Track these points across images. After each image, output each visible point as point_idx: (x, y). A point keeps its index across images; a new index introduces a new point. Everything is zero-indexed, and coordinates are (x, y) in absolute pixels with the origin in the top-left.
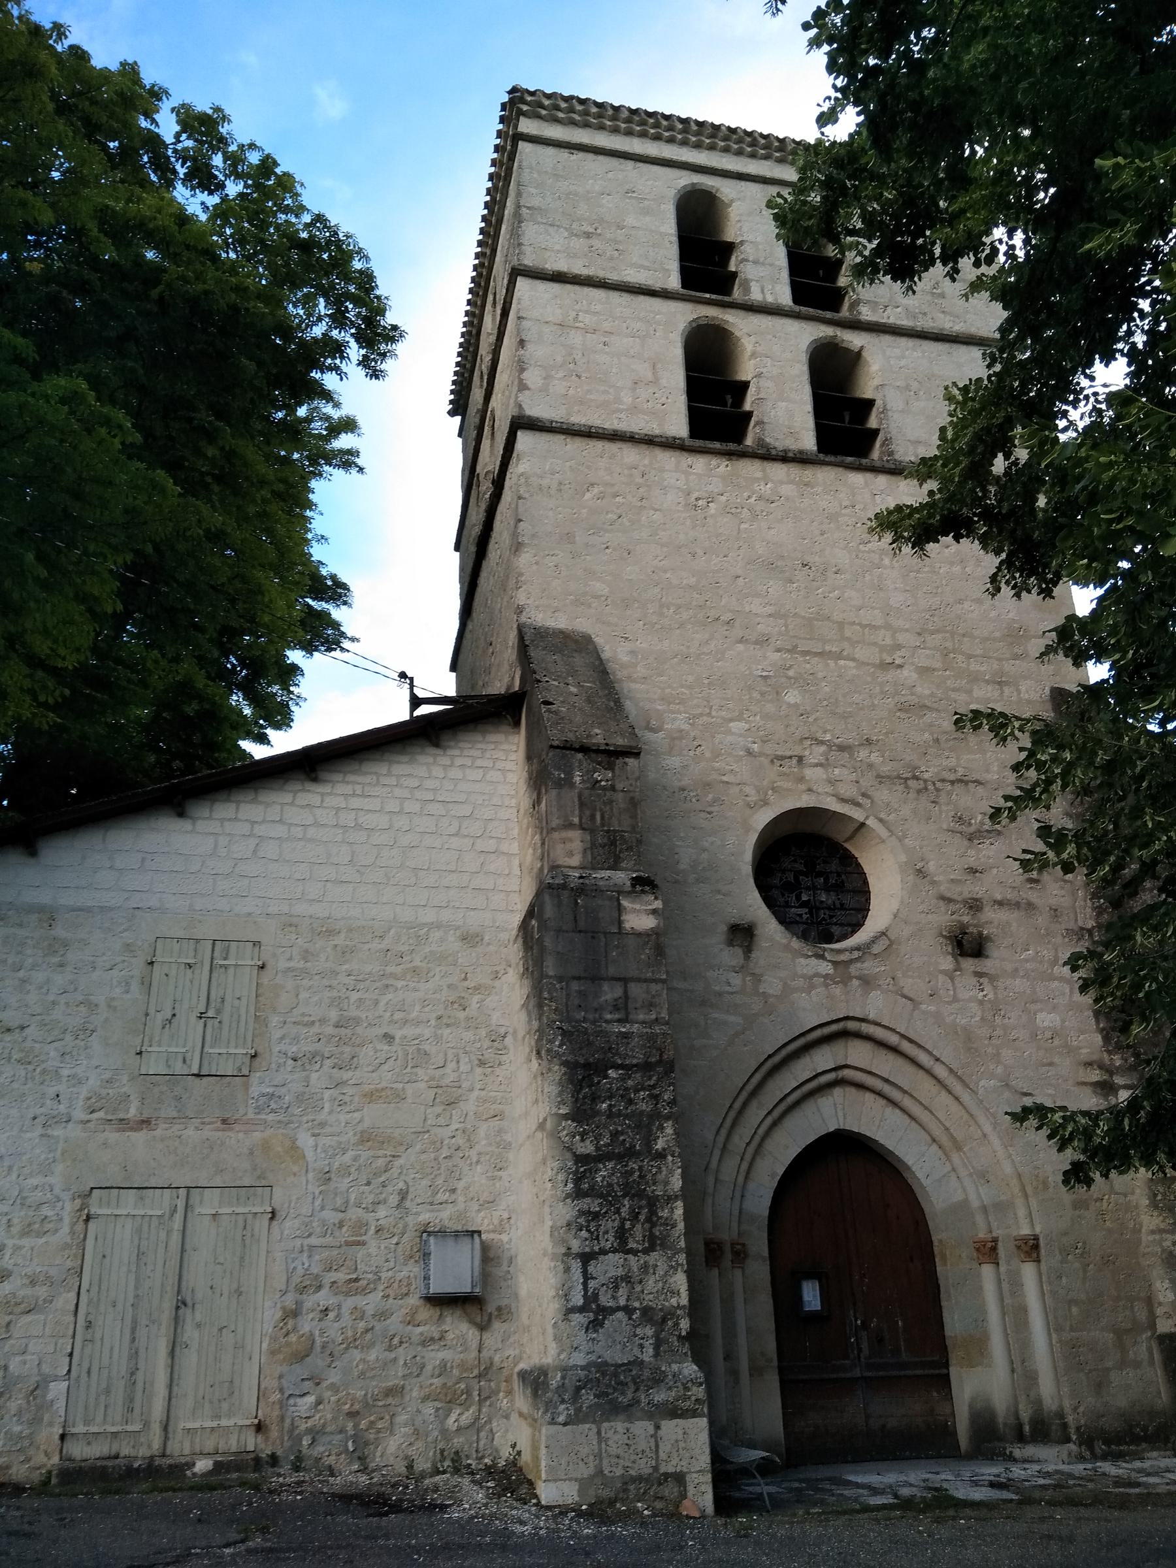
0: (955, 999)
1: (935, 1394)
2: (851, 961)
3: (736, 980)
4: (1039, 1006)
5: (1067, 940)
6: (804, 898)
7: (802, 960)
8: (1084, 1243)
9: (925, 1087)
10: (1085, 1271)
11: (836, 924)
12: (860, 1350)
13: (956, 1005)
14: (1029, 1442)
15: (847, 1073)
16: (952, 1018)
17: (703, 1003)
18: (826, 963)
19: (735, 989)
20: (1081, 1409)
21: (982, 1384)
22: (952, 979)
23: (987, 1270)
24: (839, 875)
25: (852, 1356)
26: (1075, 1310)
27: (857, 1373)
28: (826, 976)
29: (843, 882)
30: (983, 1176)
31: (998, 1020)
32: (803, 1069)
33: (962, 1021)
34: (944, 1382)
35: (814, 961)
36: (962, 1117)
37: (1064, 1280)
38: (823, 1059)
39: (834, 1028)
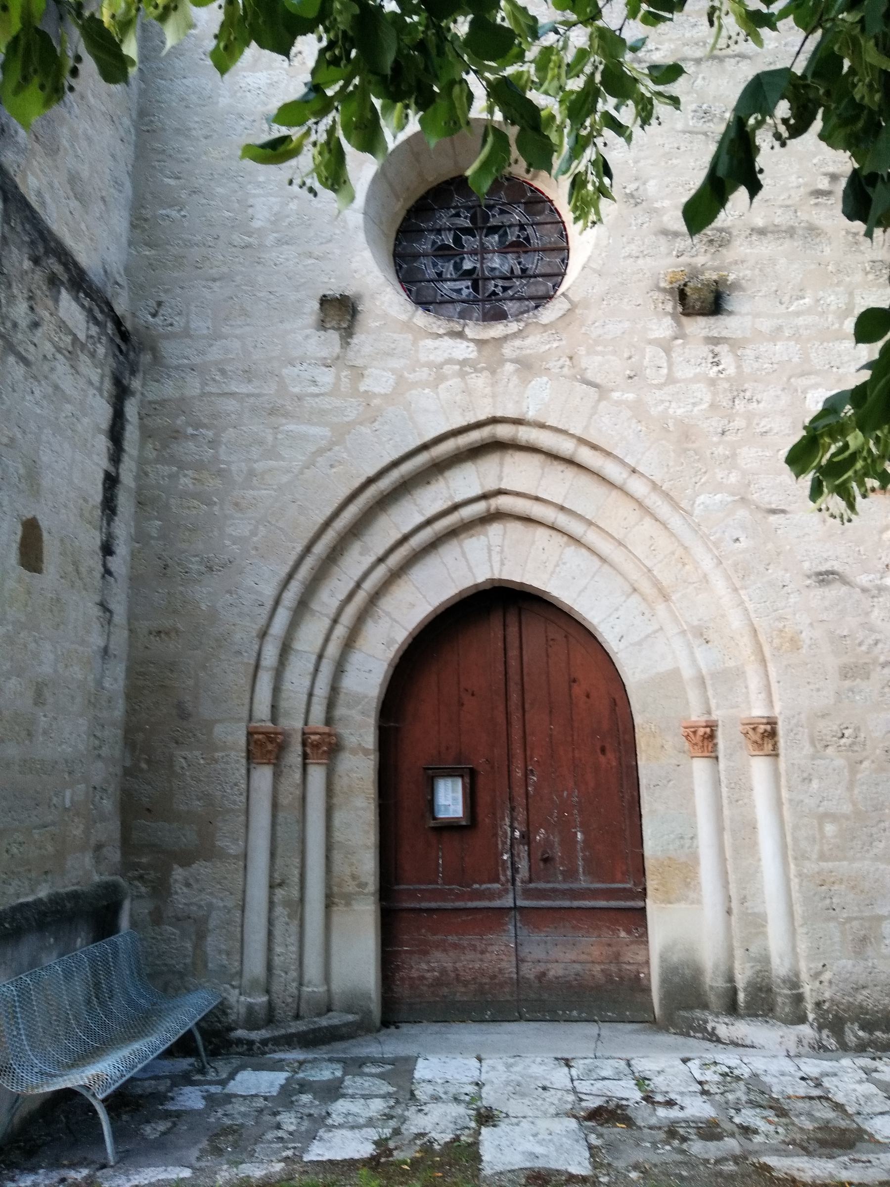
0: (671, 380)
1: (623, 934)
2: (506, 338)
3: (326, 377)
4: (813, 380)
5: (871, 277)
6: (467, 265)
7: (429, 343)
8: (857, 729)
9: (614, 514)
10: (853, 771)
11: (512, 299)
12: (515, 870)
13: (671, 389)
14: (742, 1017)
15: (503, 503)
16: (661, 408)
17: (273, 411)
18: (465, 343)
19: (323, 390)
20: (827, 976)
21: (683, 927)
22: (668, 351)
23: (700, 767)
24: (522, 227)
25: (502, 878)
26: (830, 829)
27: (508, 902)
28: (464, 363)
29: (527, 239)
30: (701, 634)
31: (740, 405)
32: (432, 499)
33: (678, 410)
34: (637, 919)
35: (448, 342)
36: (673, 553)
37: (815, 784)
38: (465, 482)
39: (475, 436)
